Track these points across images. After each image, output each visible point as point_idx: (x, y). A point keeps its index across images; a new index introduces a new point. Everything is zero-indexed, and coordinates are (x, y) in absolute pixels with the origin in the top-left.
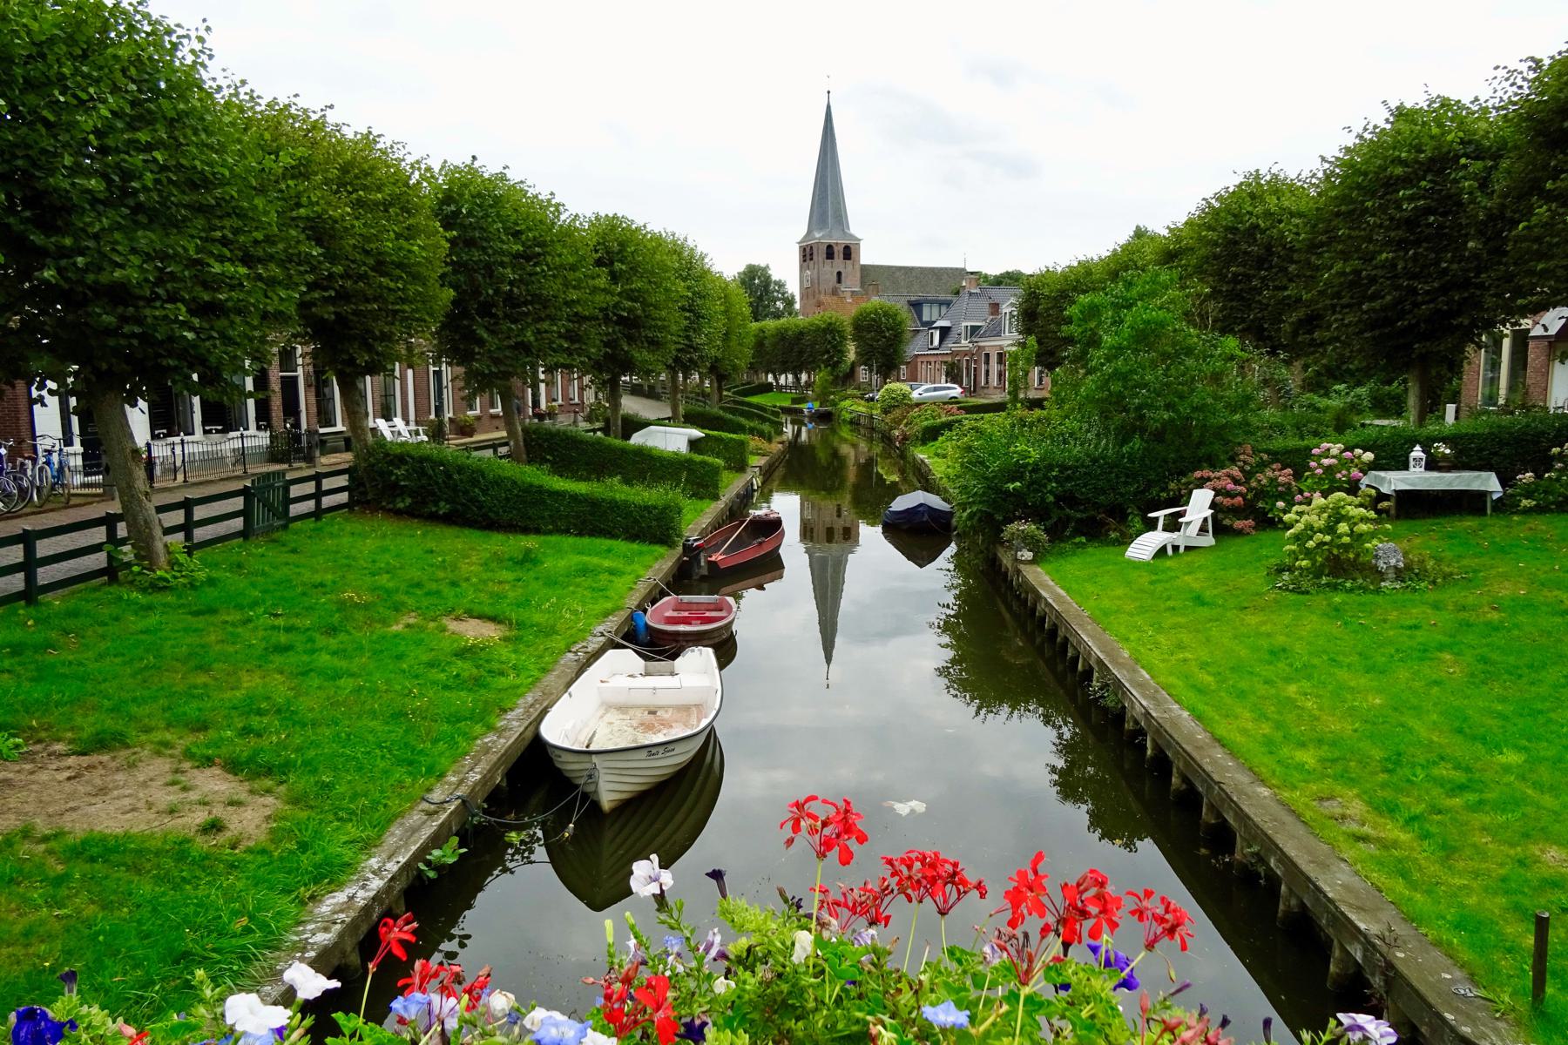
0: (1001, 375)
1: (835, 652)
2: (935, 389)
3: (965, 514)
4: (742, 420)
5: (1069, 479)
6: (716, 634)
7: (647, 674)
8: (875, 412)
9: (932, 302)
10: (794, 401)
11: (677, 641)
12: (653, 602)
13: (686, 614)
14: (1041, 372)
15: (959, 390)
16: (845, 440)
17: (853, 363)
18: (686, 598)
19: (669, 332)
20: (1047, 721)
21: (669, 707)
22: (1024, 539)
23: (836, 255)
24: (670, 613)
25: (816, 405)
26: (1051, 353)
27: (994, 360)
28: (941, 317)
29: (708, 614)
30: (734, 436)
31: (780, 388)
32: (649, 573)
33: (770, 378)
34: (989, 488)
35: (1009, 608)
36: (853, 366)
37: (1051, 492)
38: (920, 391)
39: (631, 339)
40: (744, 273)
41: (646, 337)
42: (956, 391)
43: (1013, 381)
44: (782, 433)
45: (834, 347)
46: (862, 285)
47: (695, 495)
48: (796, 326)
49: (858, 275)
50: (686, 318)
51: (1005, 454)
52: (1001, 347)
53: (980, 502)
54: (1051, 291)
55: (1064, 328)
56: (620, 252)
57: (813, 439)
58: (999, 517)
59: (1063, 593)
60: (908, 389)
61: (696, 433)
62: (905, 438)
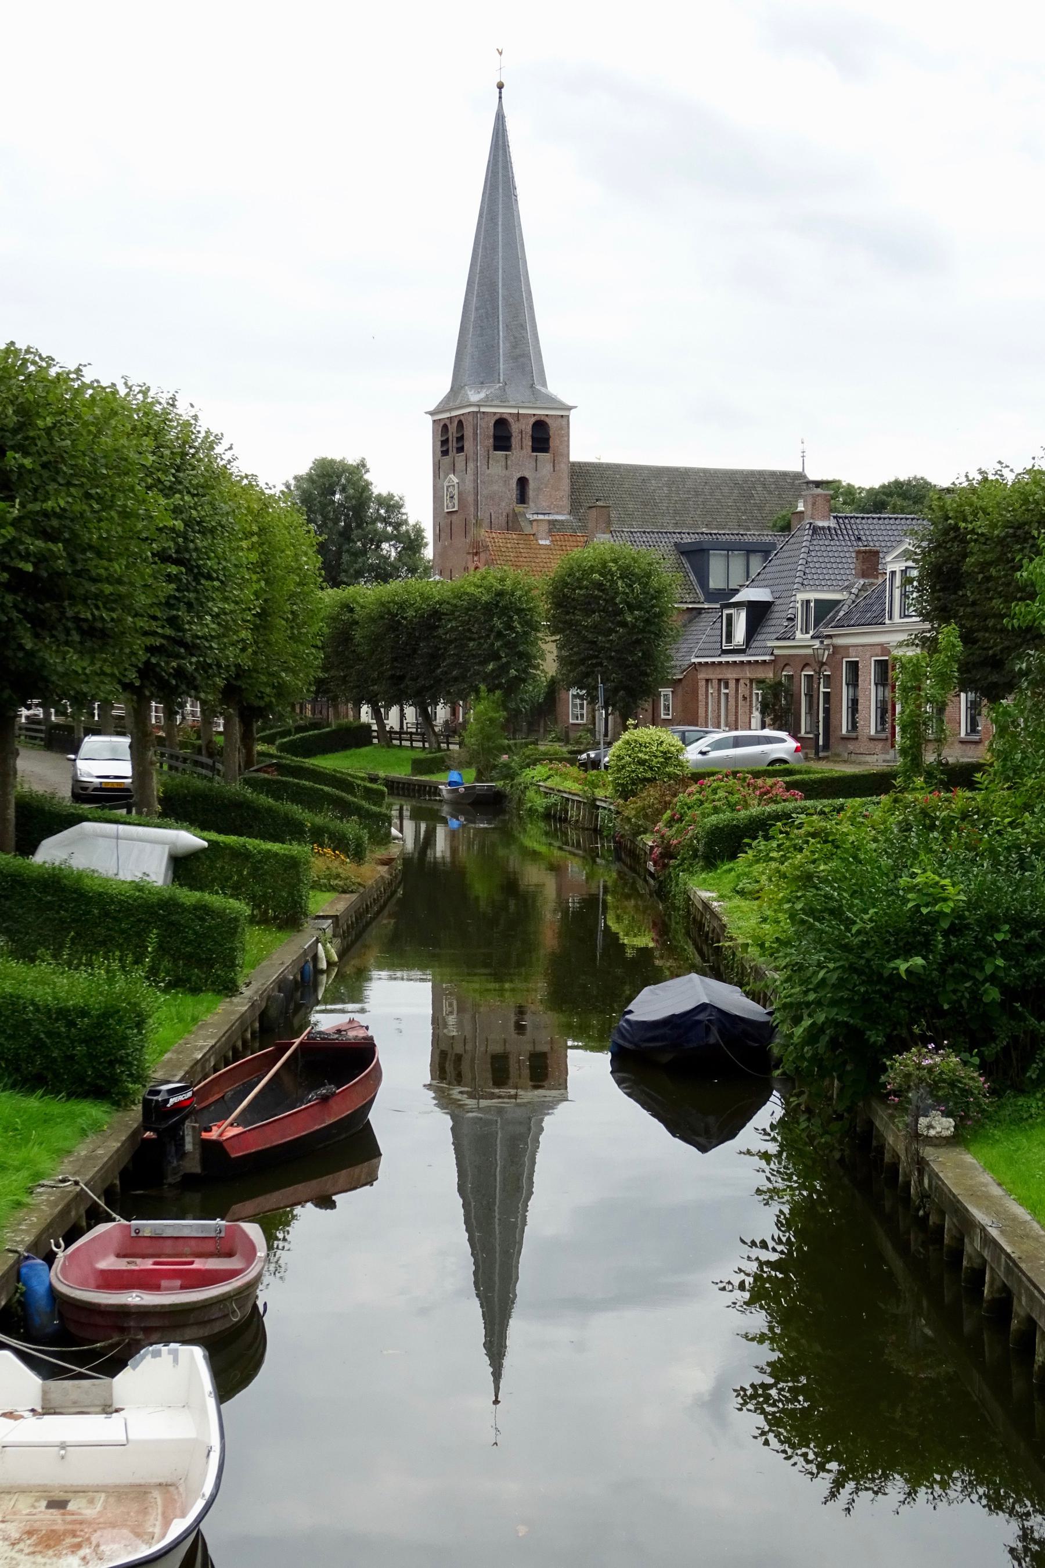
0: (884, 710)
1: (507, 1362)
2: (737, 742)
3: (799, 1031)
4: (297, 811)
5: (1031, 948)
6: (216, 1313)
7: (48, 1409)
8: (600, 793)
9: (729, 548)
10: (419, 766)
11: (122, 1330)
12: (70, 1238)
13: (148, 1264)
14: (974, 707)
15: (792, 744)
16: (535, 855)
17: (553, 683)
18: (149, 1226)
19: (128, 609)
20: (995, 1504)
21: (98, 1489)
22: (933, 1088)
23: (515, 442)
24: (109, 1263)
25: (467, 777)
26: (996, 664)
27: (868, 676)
28: (751, 581)
29: (199, 1264)
30: (275, 847)
31: (387, 737)
32: (65, 1168)
33: (366, 714)
34: (852, 969)
35: (903, 1249)
36: (553, 688)
37: (993, 979)
38: (702, 744)
39: (39, 624)
40: (310, 478)
41: (77, 619)
42: (784, 747)
43: (914, 726)
44: (386, 839)
45: (511, 645)
46: (574, 509)
47: (177, 983)
48: (425, 598)
49: (565, 485)
50: (170, 578)
51: (888, 893)
52: (884, 649)
53: (834, 1003)
54: (993, 526)
55: (1018, 608)
56: (20, 427)
57: (462, 849)
58: (876, 1037)
59: (1021, 1213)
60: (676, 740)
61: (189, 839)
62: (668, 853)
